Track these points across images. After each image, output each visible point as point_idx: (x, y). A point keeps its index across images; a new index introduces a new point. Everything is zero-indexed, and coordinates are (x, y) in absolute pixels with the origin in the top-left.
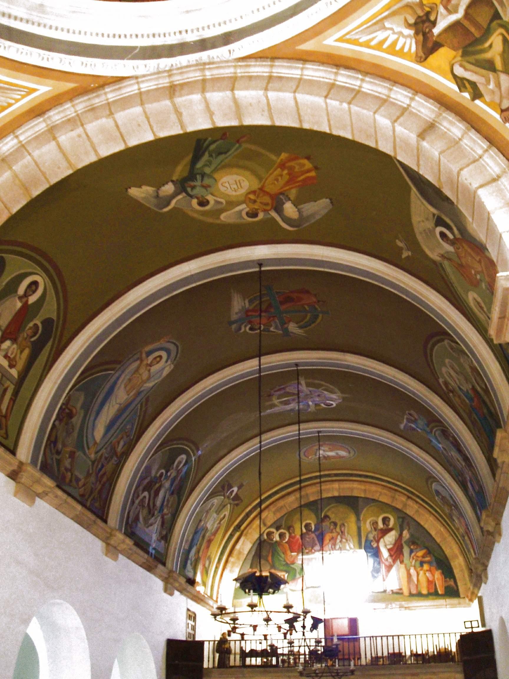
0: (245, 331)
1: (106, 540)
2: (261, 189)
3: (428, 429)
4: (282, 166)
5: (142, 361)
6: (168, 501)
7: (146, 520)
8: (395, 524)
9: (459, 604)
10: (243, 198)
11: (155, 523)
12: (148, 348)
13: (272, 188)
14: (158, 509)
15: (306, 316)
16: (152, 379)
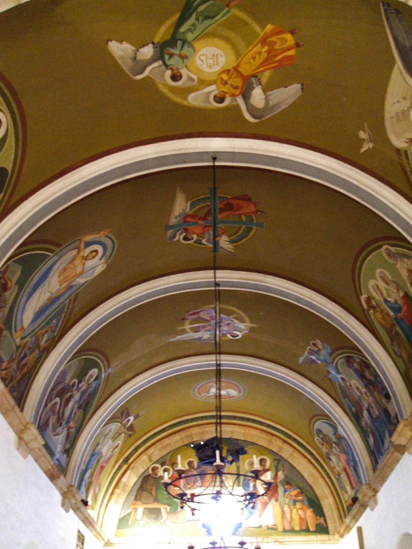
0: (179, 240)
1: (20, 434)
2: (236, 69)
3: (330, 360)
4: (264, 42)
5: (79, 252)
6: (75, 414)
7: (54, 429)
8: (271, 465)
9: (329, 540)
10: (215, 78)
11: (62, 433)
12: (88, 238)
13: (246, 70)
14: (66, 420)
15: (240, 228)
16: (84, 275)
